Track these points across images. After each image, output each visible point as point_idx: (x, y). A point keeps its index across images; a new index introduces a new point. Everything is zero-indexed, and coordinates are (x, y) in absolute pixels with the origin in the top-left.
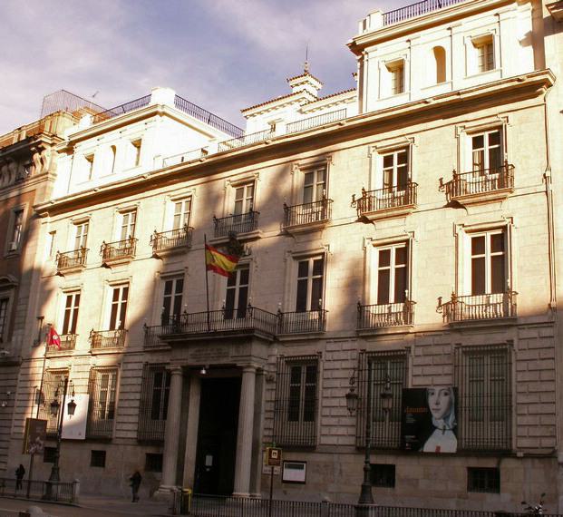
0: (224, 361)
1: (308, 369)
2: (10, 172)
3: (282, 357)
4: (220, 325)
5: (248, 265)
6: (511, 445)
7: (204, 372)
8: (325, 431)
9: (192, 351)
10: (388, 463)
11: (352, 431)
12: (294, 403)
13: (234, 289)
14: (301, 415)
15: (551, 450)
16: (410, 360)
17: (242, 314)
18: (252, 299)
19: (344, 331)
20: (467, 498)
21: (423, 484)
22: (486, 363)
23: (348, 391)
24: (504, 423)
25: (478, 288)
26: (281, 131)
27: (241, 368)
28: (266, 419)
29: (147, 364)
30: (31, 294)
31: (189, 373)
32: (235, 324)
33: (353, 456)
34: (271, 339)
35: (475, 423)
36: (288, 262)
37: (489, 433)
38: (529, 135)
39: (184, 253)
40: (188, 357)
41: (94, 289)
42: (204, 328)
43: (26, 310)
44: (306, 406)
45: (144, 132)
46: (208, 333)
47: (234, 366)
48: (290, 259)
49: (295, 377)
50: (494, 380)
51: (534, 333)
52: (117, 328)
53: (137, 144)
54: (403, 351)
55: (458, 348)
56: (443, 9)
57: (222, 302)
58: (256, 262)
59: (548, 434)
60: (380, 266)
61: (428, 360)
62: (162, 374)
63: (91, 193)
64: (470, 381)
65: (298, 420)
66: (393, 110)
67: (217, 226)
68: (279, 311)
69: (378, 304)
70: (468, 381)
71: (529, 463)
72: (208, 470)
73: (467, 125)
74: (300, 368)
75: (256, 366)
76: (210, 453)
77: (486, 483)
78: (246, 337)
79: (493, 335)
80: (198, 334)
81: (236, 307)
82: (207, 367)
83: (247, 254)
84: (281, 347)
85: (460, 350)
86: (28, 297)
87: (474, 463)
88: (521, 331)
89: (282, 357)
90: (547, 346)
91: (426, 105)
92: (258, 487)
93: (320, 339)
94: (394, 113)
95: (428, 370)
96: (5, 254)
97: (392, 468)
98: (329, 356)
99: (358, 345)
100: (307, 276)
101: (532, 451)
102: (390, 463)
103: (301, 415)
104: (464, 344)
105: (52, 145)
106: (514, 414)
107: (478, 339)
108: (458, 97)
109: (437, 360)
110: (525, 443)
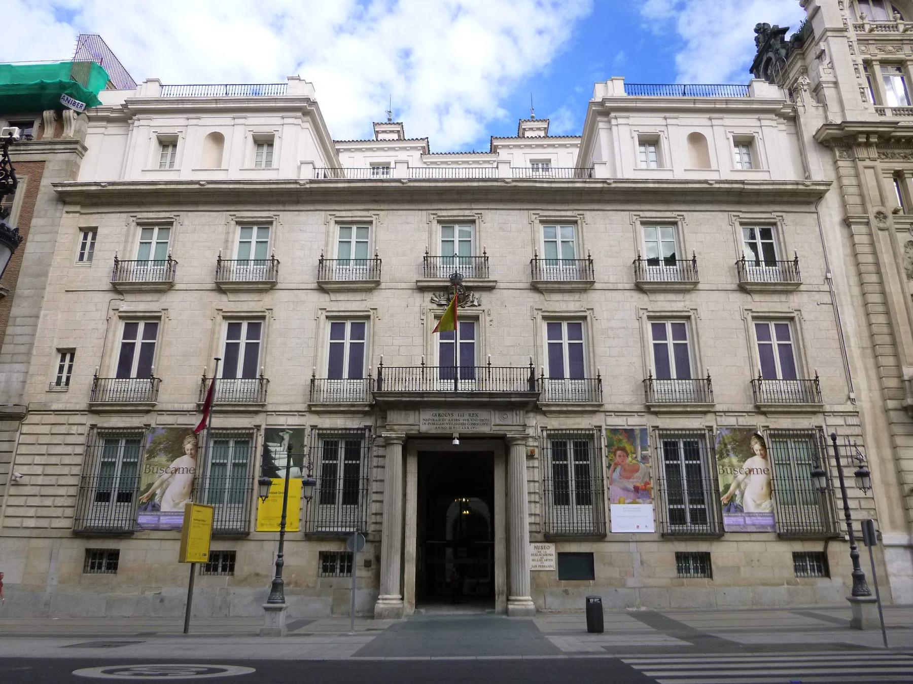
3: (93, 427)
5: (477, 318)
7: (457, 442)
11: (69, 512)
14: (340, 496)
23: (857, 469)
30: (42, 313)
33: (655, 544)
44: (577, 487)
45: (183, 129)
54: (141, 428)
56: (685, 98)
60: (124, 339)
65: (334, 503)
66: (783, 184)
69: (678, 379)
70: (210, 464)
73: (742, 215)
77: (104, 564)
79: (673, 421)
83: (476, 303)
87: (799, 547)
89: (543, 429)
93: (710, 412)
97: (589, 558)
99: (89, 420)
100: (239, 339)
102: (588, 551)
103: (573, 497)
104: (99, 425)
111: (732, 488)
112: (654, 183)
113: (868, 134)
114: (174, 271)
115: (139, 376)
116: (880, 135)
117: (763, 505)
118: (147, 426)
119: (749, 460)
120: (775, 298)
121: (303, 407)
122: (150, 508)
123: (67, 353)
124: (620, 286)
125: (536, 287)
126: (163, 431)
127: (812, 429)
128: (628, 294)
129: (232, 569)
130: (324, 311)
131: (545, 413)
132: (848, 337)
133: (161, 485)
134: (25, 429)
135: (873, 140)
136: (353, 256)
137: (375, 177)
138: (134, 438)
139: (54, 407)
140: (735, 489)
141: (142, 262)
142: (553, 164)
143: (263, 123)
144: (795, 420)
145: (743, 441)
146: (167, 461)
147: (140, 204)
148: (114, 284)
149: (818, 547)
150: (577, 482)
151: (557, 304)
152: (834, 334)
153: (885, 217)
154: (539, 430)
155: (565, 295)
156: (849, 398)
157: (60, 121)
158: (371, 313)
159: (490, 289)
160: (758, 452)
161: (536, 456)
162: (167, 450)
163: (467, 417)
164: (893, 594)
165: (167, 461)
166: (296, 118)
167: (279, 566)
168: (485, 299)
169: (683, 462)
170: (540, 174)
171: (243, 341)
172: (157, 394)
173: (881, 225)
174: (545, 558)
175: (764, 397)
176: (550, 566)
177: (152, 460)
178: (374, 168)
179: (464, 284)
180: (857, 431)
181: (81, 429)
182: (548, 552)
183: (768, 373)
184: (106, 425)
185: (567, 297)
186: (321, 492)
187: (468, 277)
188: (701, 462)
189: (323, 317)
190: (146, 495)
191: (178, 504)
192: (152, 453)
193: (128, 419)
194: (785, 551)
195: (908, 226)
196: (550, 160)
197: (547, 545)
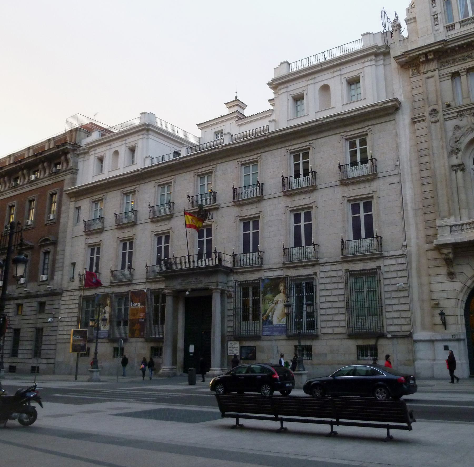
0: (201, 286)
2: (44, 169)
3: (81, 296)
5: (211, 225)
6: (383, 331)
8: (323, 324)
9: (179, 281)
10: (307, 345)
12: (245, 310)
13: (161, 247)
15: (408, 333)
16: (317, 280)
17: (209, 255)
18: (214, 246)
22: (365, 281)
24: (378, 317)
26: (226, 141)
27: (211, 290)
28: (228, 320)
29: (347, 271)
31: (177, 294)
32: (205, 263)
34: (229, 271)
35: (360, 317)
37: (367, 324)
39: (312, 191)
40: (177, 285)
41: (2, 263)
42: (186, 266)
43: (64, 259)
46: (189, 269)
47: (207, 289)
49: (245, 294)
50: (371, 291)
52: (126, 267)
53: (132, 150)
55: (347, 272)
57: (196, 250)
59: (406, 323)
61: (328, 280)
62: (159, 296)
64: (355, 292)
67: (190, 201)
68: (233, 253)
69: (354, 240)
71: (395, 341)
72: (191, 355)
73: (345, 134)
75: (221, 288)
76: (192, 344)
77: (369, 354)
78: (214, 271)
79: (369, 264)
80: (182, 270)
81: (205, 252)
82: (190, 290)
83: (210, 218)
84: (235, 276)
85: (348, 273)
86: (64, 250)
87: (360, 342)
88: (385, 260)
90: (401, 269)
92: (226, 364)
94: (300, 128)
95: (328, 286)
96: (46, 223)
98: (322, 275)
101: (398, 334)
104: (350, 269)
106: (384, 311)
107: (359, 266)
109: (334, 280)
110: (392, 329)
111: (268, 311)
113: (426, 54)
114: (376, 166)
115: (306, 245)
116: (435, 52)
117: (282, 321)
120: (362, 185)
121: (339, 259)
122: (267, 323)
123: (74, 264)
124: (276, 195)
127: (258, 280)
128: (280, 199)
130: (288, 208)
131: (237, 273)
132: (406, 204)
134: (63, 299)
135: (430, 57)
136: (251, 184)
139: (70, 288)
140: (270, 312)
141: (246, 187)
143: (350, 71)
144: (365, 264)
145: (274, 285)
146: (273, 297)
147: (92, 192)
148: (340, 181)
149: (372, 342)
151: (246, 211)
152: (398, 203)
153: (437, 112)
155: (250, 205)
156: (403, 246)
157: (67, 161)
159: (217, 209)
160: (282, 291)
161: (233, 296)
163: (194, 280)
164: (416, 371)
165: (273, 297)
166: (371, 60)
168: (215, 214)
169: (304, 294)
171: (362, 214)
172: (318, 254)
173: (434, 119)
174: (235, 349)
179: (204, 209)
180: (404, 267)
181: (340, 273)
185: (251, 206)
186: (243, 316)
187: (207, 203)
189: (346, 202)
190: (265, 316)
192: (265, 293)
194: (352, 345)
195: (456, 114)
197: (235, 342)
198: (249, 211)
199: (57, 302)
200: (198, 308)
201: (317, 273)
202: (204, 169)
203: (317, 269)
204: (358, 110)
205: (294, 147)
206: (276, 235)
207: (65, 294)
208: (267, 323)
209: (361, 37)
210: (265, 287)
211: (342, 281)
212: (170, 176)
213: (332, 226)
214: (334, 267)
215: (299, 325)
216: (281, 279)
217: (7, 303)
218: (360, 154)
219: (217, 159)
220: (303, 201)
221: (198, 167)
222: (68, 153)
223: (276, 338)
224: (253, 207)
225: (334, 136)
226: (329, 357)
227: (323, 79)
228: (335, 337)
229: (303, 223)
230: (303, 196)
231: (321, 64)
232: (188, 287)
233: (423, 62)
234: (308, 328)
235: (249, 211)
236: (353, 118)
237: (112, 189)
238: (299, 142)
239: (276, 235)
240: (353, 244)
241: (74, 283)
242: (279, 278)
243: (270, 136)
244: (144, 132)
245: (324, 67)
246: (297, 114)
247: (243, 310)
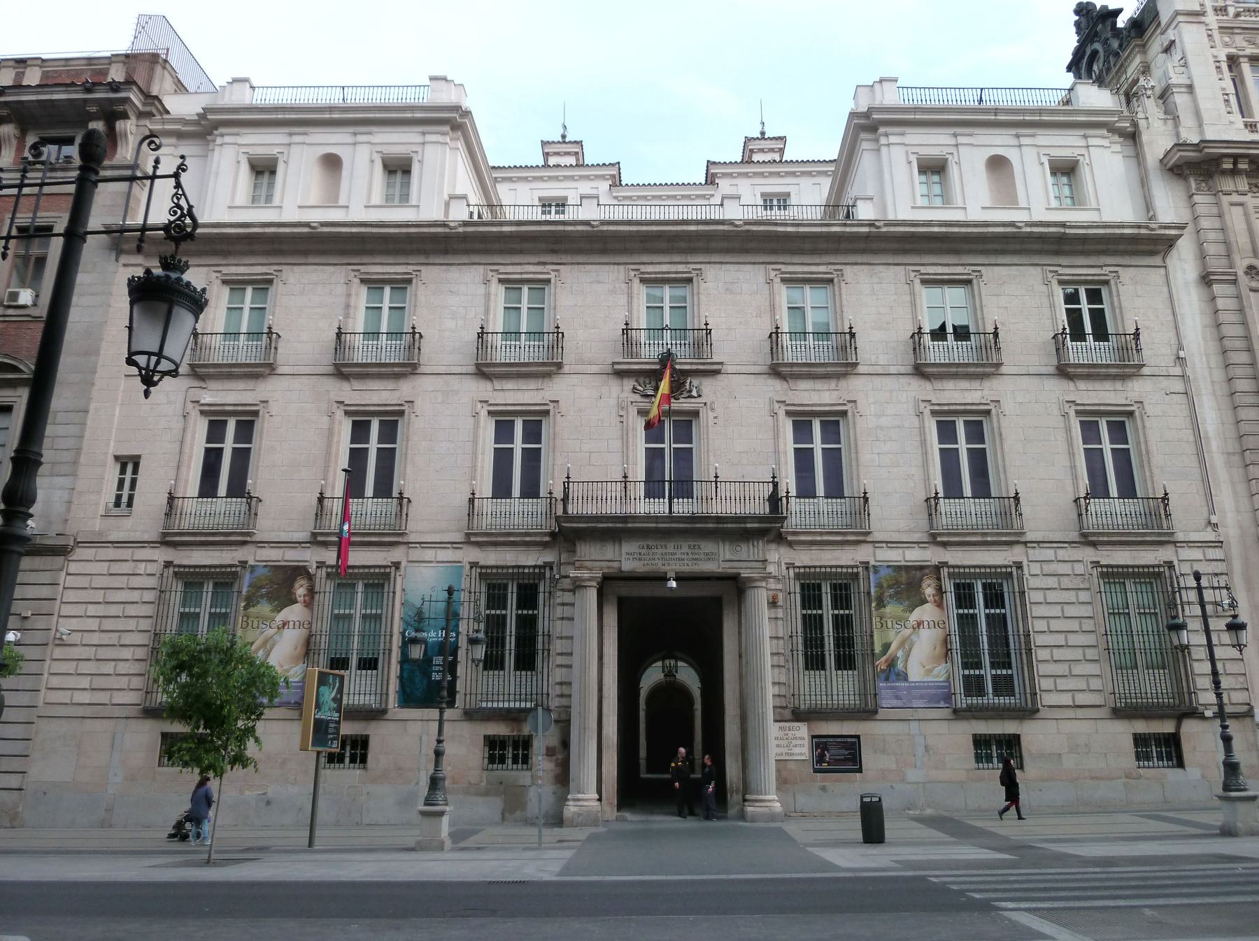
1: (834, 587)
4: (643, 506)
5: (696, 414)
15: (1245, 708)
19: (910, 531)
20: (1139, 777)
21: (1069, 762)
25: (208, 487)
36: (191, 420)
38: (1162, 307)
44: (837, 645)
48: (339, 414)
51: (1048, 554)
58: (712, 409)
63: (580, 228)
69: (826, 497)
73: (1061, 271)
74: (819, 586)
79: (1143, 554)
83: (694, 393)
85: (791, 571)
87: (1142, 727)
91: (1015, 230)
98: (1035, 569)
103: (830, 661)
105: (141, 115)
107: (1122, 557)
108: (1062, 230)
111: (893, 647)
112: (940, 226)
113: (1236, 158)
115: (230, 494)
117: (936, 671)
118: (243, 564)
119: (918, 610)
120: (1108, 385)
123: (129, 463)
125: (777, 371)
126: (266, 570)
127: (1159, 566)
128: (903, 380)
129: (364, 760)
131: (790, 544)
132: (1207, 438)
133: (265, 642)
135: (1243, 166)
137: (548, 218)
138: (224, 579)
140: (898, 648)
142: (793, 200)
145: (907, 584)
146: (272, 611)
147: (226, 254)
148: (477, 365)
149: (1167, 727)
150: (837, 639)
152: (1188, 435)
154: (784, 567)
155: (818, 381)
156: (1209, 523)
158: (551, 407)
160: (300, 599)
162: (270, 597)
163: (685, 549)
165: (272, 611)
167: (438, 754)
168: (708, 387)
169: (981, 611)
170: (776, 214)
171: (373, 445)
174: (794, 742)
175: (1091, 522)
176: (801, 754)
177: (251, 610)
178: (544, 206)
182: (798, 734)
183: (1098, 489)
184: (185, 562)
185: (819, 385)
188: (831, 612)
191: (931, 671)
192: (250, 601)
193: (217, 554)
194: (1123, 732)
196: (788, 194)
198: (377, 394)
199: (45, 577)
200: (675, 628)
201: (399, 563)
202: (665, 268)
203: (397, 554)
204: (629, 223)
205: (931, 270)
206: (893, 459)
207: (80, 553)
208: (893, 677)
209: (428, 83)
210: (255, 587)
211: (1087, 586)
212: (545, 264)
213: (1040, 460)
214: (1062, 554)
215: (974, 686)
216: (927, 571)
217: (26, 562)
218: (1088, 317)
219: (707, 251)
220: (966, 394)
221: (645, 258)
222: (125, 116)
223: (921, 714)
224: (826, 387)
225: (1031, 268)
226: (1069, 762)
227: (334, 141)
228: (1080, 713)
229: (228, 445)
230: (964, 384)
231: (331, 109)
232: (666, 568)
233: (1224, 173)
234: (997, 692)
235: (377, 394)
236: (1084, 239)
237: (311, 260)
238: (264, 261)
239: (893, 459)
240: (487, 506)
241: (127, 523)
242: (922, 568)
243: (884, 229)
244: (447, 128)
245: (1001, 117)
246: (332, 198)
247: (805, 641)
